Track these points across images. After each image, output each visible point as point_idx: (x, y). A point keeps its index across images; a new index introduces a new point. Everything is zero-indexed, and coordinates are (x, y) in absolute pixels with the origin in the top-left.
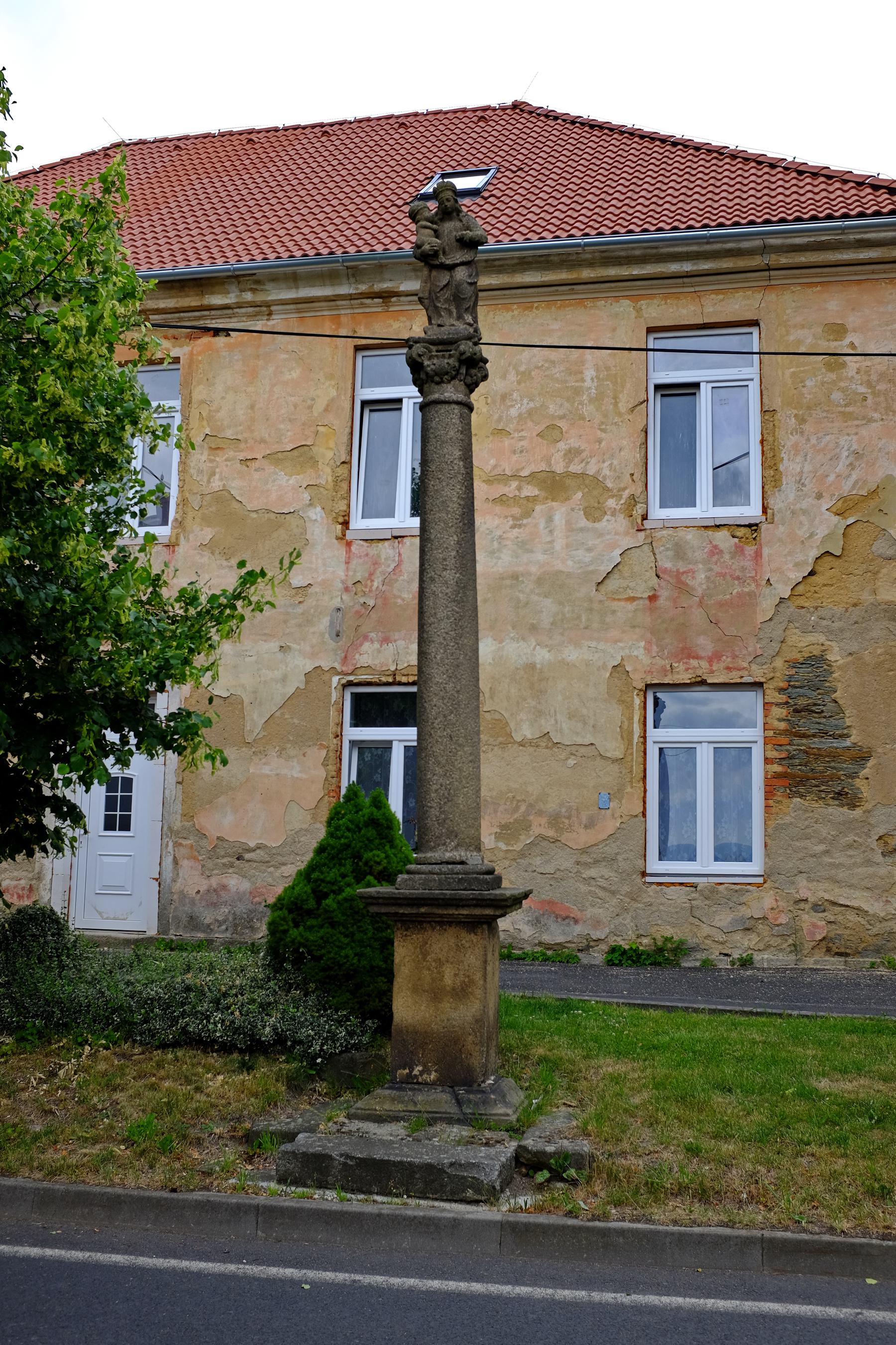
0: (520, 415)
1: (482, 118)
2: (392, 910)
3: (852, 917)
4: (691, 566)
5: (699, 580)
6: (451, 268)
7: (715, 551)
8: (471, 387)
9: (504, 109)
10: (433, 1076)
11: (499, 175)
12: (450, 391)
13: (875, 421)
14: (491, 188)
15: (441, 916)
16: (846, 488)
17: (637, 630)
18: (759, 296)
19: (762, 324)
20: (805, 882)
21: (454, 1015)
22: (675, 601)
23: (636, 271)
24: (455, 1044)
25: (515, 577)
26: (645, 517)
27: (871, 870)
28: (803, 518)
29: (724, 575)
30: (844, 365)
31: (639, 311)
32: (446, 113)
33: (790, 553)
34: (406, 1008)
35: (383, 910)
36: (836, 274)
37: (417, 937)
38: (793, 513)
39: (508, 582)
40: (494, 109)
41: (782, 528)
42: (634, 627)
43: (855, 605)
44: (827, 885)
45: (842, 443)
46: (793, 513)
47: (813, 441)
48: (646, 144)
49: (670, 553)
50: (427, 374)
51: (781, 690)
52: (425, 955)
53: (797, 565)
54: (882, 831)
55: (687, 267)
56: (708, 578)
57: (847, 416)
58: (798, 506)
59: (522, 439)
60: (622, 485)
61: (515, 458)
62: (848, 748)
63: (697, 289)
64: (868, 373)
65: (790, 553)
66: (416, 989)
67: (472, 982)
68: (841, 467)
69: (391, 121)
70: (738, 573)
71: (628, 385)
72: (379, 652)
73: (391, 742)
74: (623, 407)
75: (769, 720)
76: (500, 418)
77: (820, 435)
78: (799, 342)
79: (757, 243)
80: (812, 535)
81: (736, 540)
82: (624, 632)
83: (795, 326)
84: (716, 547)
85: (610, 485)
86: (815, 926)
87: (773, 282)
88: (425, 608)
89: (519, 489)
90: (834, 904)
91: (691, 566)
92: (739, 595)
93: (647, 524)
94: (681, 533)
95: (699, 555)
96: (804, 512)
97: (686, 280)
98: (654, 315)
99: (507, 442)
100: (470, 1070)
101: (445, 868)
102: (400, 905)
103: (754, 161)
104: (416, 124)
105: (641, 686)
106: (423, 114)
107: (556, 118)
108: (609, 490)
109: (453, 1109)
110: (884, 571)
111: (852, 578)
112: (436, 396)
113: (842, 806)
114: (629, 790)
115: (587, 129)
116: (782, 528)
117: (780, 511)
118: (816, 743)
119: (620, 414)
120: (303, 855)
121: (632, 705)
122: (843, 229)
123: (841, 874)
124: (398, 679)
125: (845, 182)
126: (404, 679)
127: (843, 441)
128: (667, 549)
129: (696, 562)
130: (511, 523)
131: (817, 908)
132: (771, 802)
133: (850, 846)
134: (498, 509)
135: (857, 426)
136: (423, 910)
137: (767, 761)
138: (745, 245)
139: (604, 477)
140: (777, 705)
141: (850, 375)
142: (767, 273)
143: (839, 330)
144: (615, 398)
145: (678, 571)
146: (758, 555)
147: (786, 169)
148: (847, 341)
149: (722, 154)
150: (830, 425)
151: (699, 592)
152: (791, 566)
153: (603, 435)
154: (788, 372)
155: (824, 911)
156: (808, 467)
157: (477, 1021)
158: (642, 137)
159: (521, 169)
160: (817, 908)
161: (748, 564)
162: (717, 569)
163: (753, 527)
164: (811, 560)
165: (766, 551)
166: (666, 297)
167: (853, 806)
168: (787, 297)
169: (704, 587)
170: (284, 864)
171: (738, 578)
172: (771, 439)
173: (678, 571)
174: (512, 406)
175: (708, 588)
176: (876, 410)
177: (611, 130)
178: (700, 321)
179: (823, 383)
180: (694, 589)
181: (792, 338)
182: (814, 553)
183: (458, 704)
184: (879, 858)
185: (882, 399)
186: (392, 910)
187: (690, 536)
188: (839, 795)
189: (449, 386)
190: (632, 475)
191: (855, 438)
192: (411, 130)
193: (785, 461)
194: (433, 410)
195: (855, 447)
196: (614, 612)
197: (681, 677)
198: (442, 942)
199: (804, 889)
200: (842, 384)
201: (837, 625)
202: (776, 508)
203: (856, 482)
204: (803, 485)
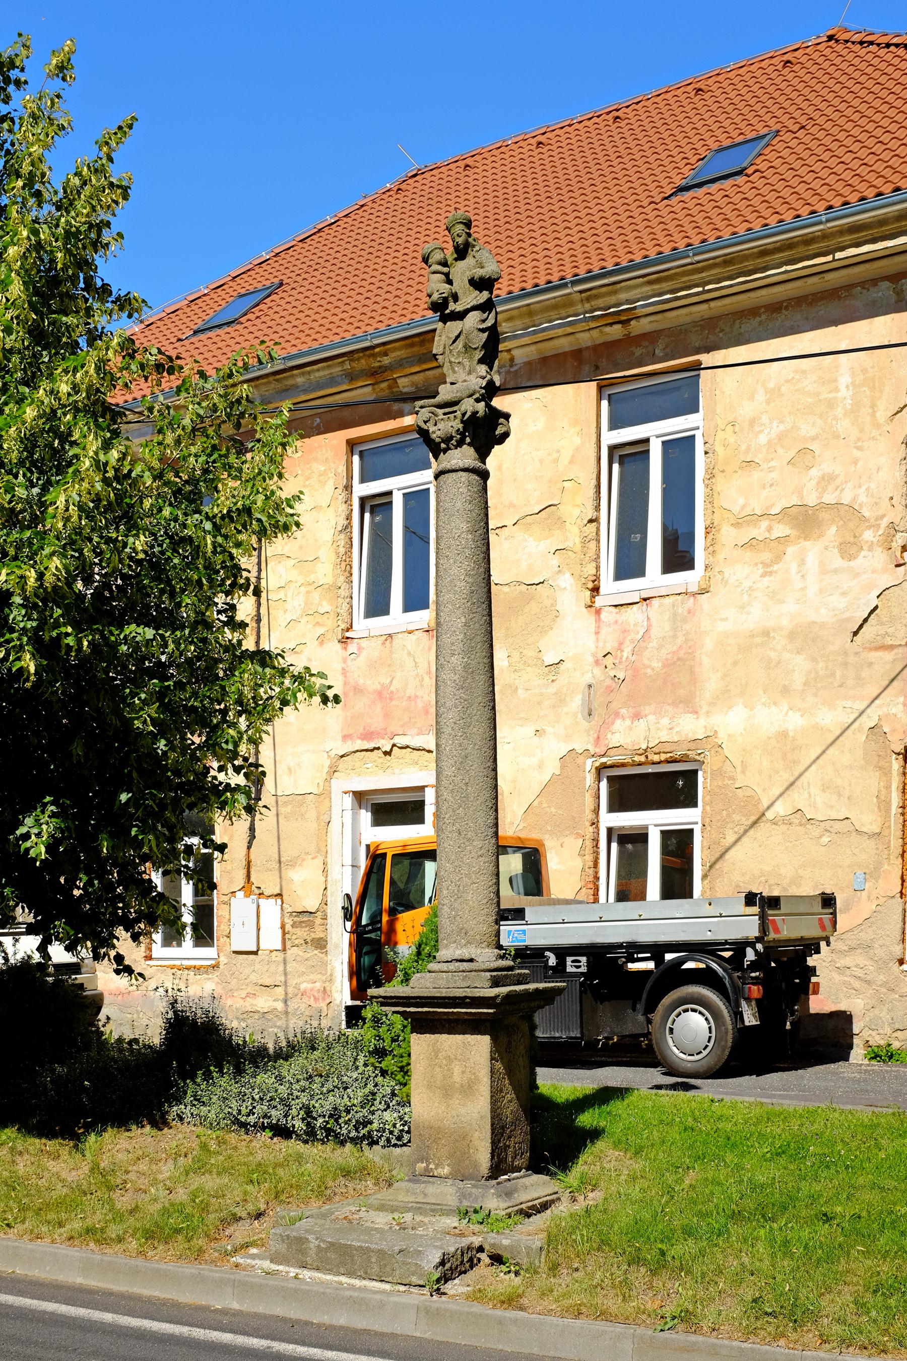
0: (769, 441)
10: (446, 1170)
21: (462, 1111)
25: (766, 633)
39: (759, 640)
59: (771, 470)
60: (880, 513)
73: (646, 827)
76: (749, 447)
89: (769, 529)
99: (756, 475)
114: (886, 867)
119: (877, 426)
126: (656, 758)
130: (761, 571)
134: (748, 555)
144: (873, 406)
174: (761, 432)
196: (870, 664)
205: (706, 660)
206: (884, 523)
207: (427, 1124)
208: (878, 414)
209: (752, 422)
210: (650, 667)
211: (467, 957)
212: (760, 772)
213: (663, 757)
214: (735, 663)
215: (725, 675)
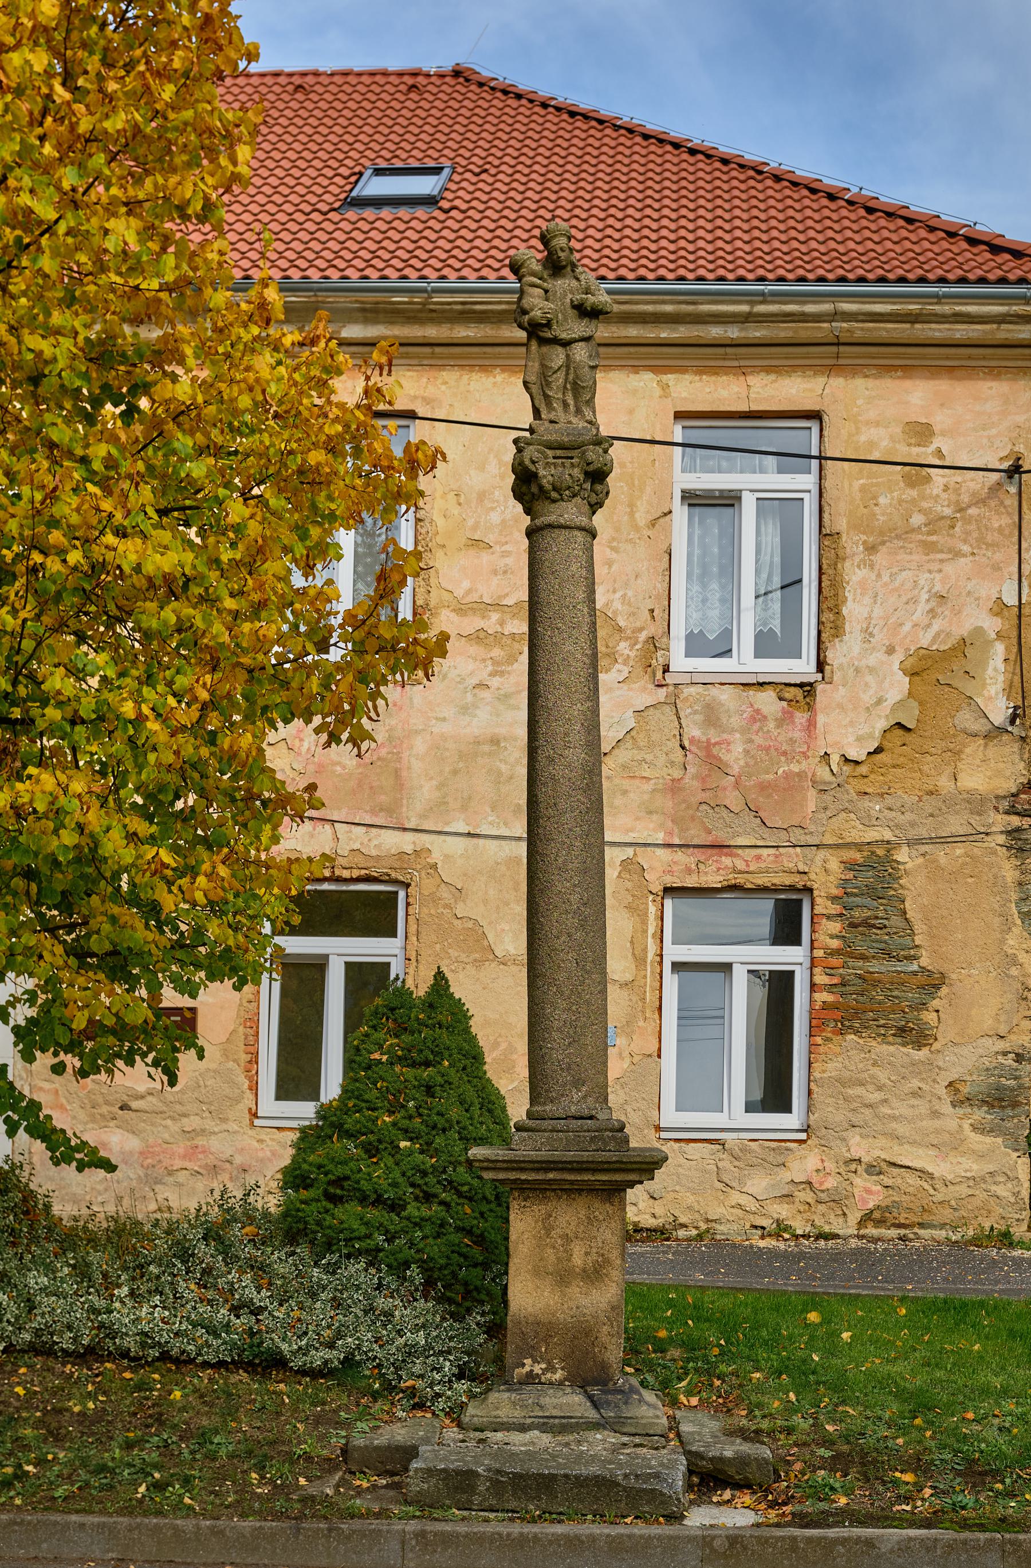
0: (503, 521)
1: (413, 87)
2: (512, 1176)
3: (912, 1180)
4: (725, 736)
5: (735, 756)
6: (566, 344)
7: (757, 717)
8: (595, 507)
9: (442, 76)
10: (558, 1375)
11: (456, 178)
12: (570, 512)
13: (964, 556)
14: (449, 195)
15: (572, 1182)
16: (925, 640)
17: (655, 817)
18: (821, 380)
19: (825, 418)
20: (858, 1138)
21: (584, 1301)
22: (703, 780)
23: (665, 333)
24: (587, 1335)
25: (495, 741)
26: (666, 669)
27: (937, 1123)
28: (869, 678)
29: (767, 749)
30: (928, 479)
31: (665, 387)
32: (359, 74)
33: (852, 723)
34: (527, 1295)
35: (501, 1176)
36: (924, 357)
37: (539, 1209)
38: (857, 670)
39: (486, 748)
40: (428, 75)
41: (842, 691)
42: (651, 813)
43: (931, 793)
44: (882, 1142)
45: (922, 582)
46: (857, 670)
47: (886, 578)
48: (653, 148)
49: (699, 718)
50: (541, 488)
51: (834, 899)
52: (548, 1230)
53: (859, 739)
54: (953, 1076)
55: (733, 333)
56: (747, 752)
57: (929, 548)
58: (863, 663)
59: (506, 554)
60: (638, 624)
61: (495, 581)
62: (915, 973)
63: (742, 363)
64: (957, 491)
65: (852, 723)
66: (537, 1272)
67: (607, 1261)
68: (920, 613)
69: (282, 80)
70: (785, 747)
71: (648, 490)
72: (312, 836)
73: (326, 957)
74: (642, 518)
75: (816, 936)
76: (477, 523)
77: (895, 570)
78: (872, 444)
79: (826, 307)
80: (880, 701)
81: (784, 704)
82: (637, 819)
83: (868, 423)
84: (758, 711)
85: (622, 624)
86: (869, 1191)
87: (841, 362)
88: (541, 797)
89: (502, 623)
90: (894, 1165)
91: (725, 736)
92: (787, 775)
93: (670, 679)
94: (714, 691)
95: (735, 721)
96: (871, 670)
97: (729, 350)
98: (684, 395)
99: (485, 557)
100: (604, 1366)
101: (575, 1124)
102: (522, 1170)
103: (807, 187)
104: (319, 89)
105: (657, 888)
106: (325, 74)
107: (519, 96)
108: (620, 630)
109: (592, 1414)
110: (968, 750)
111: (929, 758)
112: (552, 518)
113: (904, 1045)
114: (641, 1023)
115: (565, 116)
116: (842, 691)
117: (841, 667)
118: (874, 966)
119: (637, 528)
120: (211, 1103)
121: (646, 914)
122: (938, 298)
123: (901, 1129)
124: (337, 873)
125: (932, 229)
126: (346, 874)
127: (924, 578)
128: (695, 712)
129: (733, 731)
130: (490, 668)
131: (872, 1169)
132: (819, 1040)
133: (914, 1094)
134: (473, 649)
135: (942, 561)
136: (551, 1176)
137: (813, 987)
138: (810, 308)
139: (615, 612)
140: (829, 917)
141: (935, 492)
142: (834, 349)
143: (922, 432)
144: (631, 505)
145: (708, 741)
146: (811, 724)
147: (850, 202)
148: (933, 447)
149: (760, 172)
150: (908, 557)
151: (735, 770)
152: (851, 739)
153: (614, 556)
154: (858, 484)
155: (880, 1173)
156: (878, 612)
157: (613, 1308)
158: (646, 137)
159: (486, 171)
160: (872, 1169)
161: (797, 735)
162: (759, 740)
163: (807, 688)
164: (878, 734)
165: (821, 719)
166: (701, 371)
167: (919, 1046)
168: (859, 383)
169: (742, 763)
170: (185, 1115)
171: (785, 753)
172: (831, 572)
173: (708, 741)
174: (493, 509)
175: (747, 764)
176: (965, 541)
177: (601, 122)
178: (744, 408)
179: (901, 501)
180: (727, 766)
181: (863, 438)
182: (882, 724)
183: (585, 920)
184: (947, 1109)
185: (973, 527)
186: (512, 1176)
187: (725, 696)
188: (902, 1031)
189: (570, 505)
190: (652, 611)
191: (938, 577)
192: (314, 97)
193: (849, 603)
194: (548, 536)
195: (938, 587)
196: (625, 792)
197: (710, 878)
198: (568, 1216)
199: (859, 1147)
200: (925, 505)
201: (909, 816)
202: (836, 664)
203: (938, 634)
204: (871, 635)
205: (417, 765)
206: (643, 636)
207: (531, 1319)
208: (637, 515)
209: (482, 496)
210: (339, 763)
211: (586, 1112)
212: (485, 902)
213: (356, 873)
214: (455, 772)
215: (441, 786)
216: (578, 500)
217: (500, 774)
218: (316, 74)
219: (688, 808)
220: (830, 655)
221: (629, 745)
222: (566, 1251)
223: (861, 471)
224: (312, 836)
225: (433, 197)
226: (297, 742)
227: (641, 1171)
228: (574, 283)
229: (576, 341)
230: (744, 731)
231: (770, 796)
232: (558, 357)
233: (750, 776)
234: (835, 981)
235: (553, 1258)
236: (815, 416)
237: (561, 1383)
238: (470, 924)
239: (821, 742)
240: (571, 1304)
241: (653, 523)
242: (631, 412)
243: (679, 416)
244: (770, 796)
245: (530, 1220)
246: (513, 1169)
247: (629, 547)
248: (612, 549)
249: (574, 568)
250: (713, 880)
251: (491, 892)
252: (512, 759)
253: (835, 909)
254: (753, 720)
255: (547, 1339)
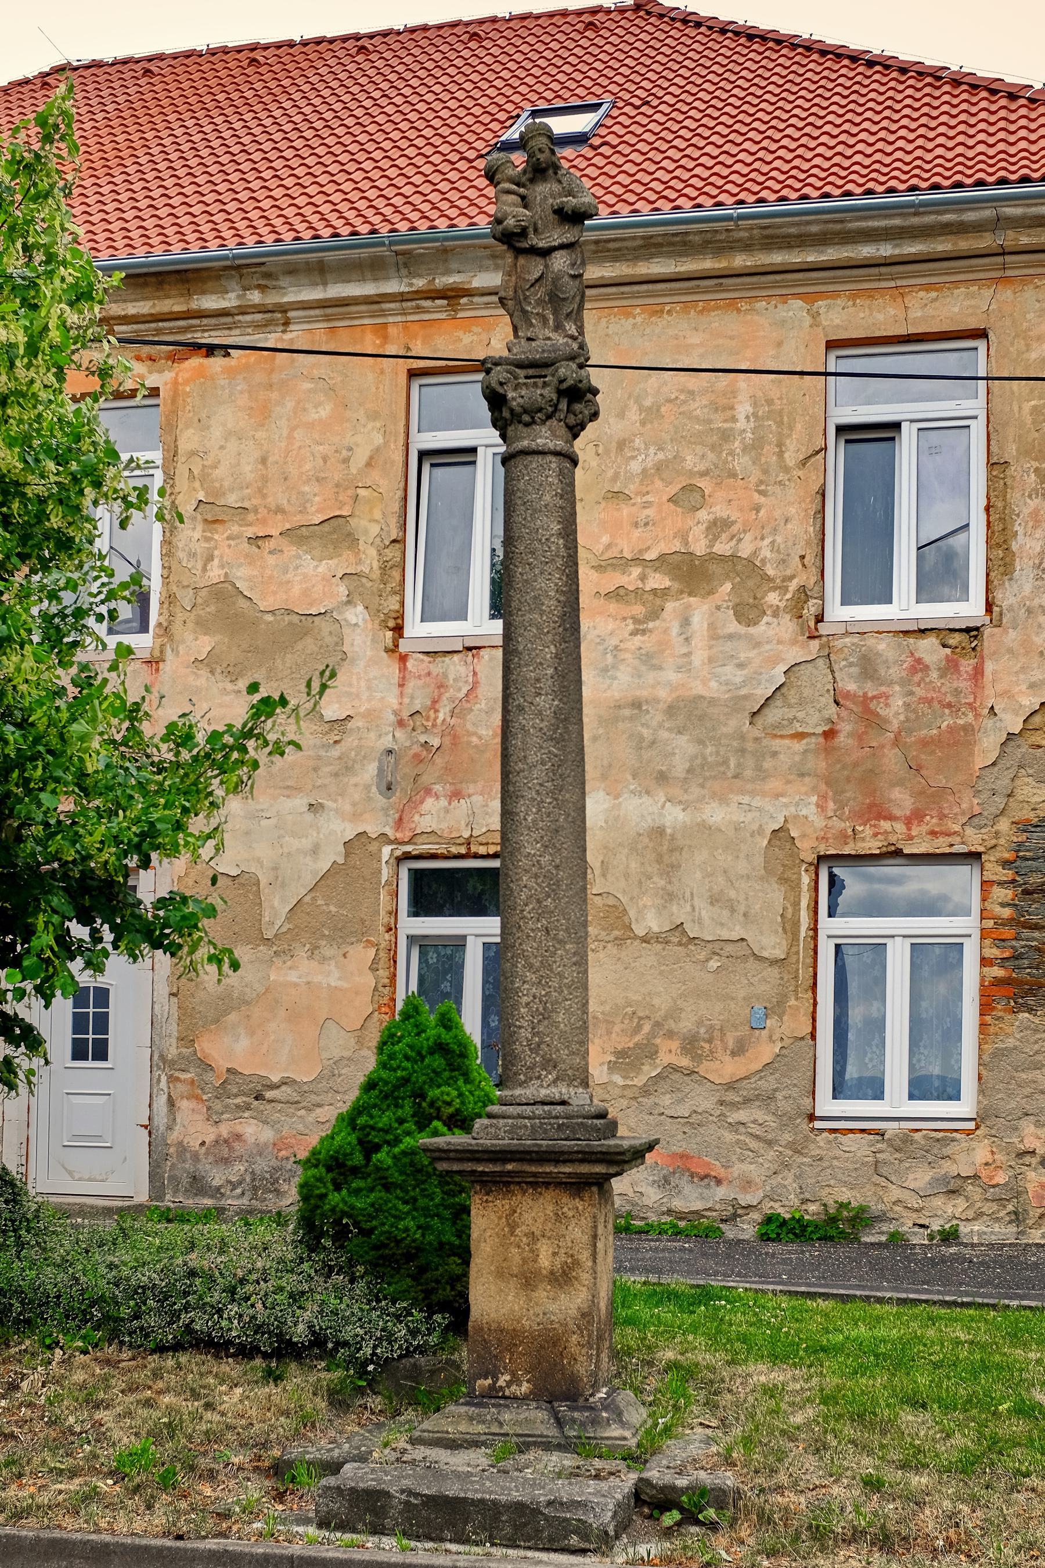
0: (644, 471)
2: (468, 1166)
4: (883, 689)
5: (894, 709)
6: (545, 253)
7: (919, 666)
8: (575, 431)
9: (622, 11)
10: (525, 1387)
11: (615, 113)
12: (545, 437)
14: (603, 131)
15: (535, 1175)
17: (807, 779)
18: (987, 293)
19: (991, 335)
20: (1032, 1128)
21: (553, 1307)
25: (637, 705)
26: (820, 619)
29: (929, 701)
31: (815, 315)
32: (538, 17)
34: (489, 1299)
35: (456, 1167)
37: (503, 1204)
38: (1029, 611)
39: (627, 712)
40: (608, 12)
46: (1029, 611)
50: (512, 410)
51: (1006, 864)
52: (513, 1227)
55: (886, 250)
56: (907, 705)
59: (647, 505)
60: (788, 572)
61: (637, 533)
63: (899, 283)
65: (1023, 669)
67: (577, 1263)
70: (949, 698)
72: (447, 811)
73: (464, 937)
74: (791, 458)
79: (988, 213)
81: (948, 651)
82: (788, 782)
84: (919, 661)
88: (511, 750)
89: (643, 578)
91: (883, 689)
92: (951, 729)
94: (870, 641)
97: (883, 270)
98: (837, 321)
99: (626, 511)
101: (539, 1110)
102: (479, 1160)
105: (811, 857)
106: (503, 19)
107: (698, 25)
108: (770, 579)
109: (551, 1431)
114: (793, 1002)
115: (742, 40)
117: (1011, 609)
119: (786, 469)
124: (474, 849)
126: (482, 850)
128: (851, 664)
129: (892, 683)
130: (631, 627)
132: (988, 1018)
134: (613, 607)
136: (509, 1167)
137: (984, 962)
138: (970, 216)
140: (1000, 884)
144: (780, 445)
146: (978, 672)
152: (1024, 687)
153: (763, 500)
154: (1027, 407)
157: (584, 1315)
158: (823, 53)
159: (647, 103)
161: (964, 684)
162: (920, 692)
163: (972, 632)
165: (989, 667)
169: (902, 718)
170: (320, 1106)
171: (949, 705)
174: (633, 458)
175: (907, 720)
178: (902, 331)
183: (558, 884)
187: (883, 646)
194: (520, 463)
196: (775, 754)
197: (867, 845)
198: (535, 1211)
206: (793, 585)
209: (621, 445)
210: (475, 734)
212: (627, 876)
216: (554, 422)
217: (641, 739)
218: (494, 20)
219: (844, 768)
220: (999, 595)
221: (779, 703)
222: (532, 1251)
223: (1032, 391)
224: (447, 811)
225: (584, 134)
226: (432, 713)
227: (610, 1162)
228: (556, 187)
229: (554, 249)
230: (903, 682)
231: (933, 752)
232: (535, 268)
233: (910, 731)
234: (1006, 955)
235: (517, 1259)
236: (982, 334)
237: (525, 1398)
238: (611, 901)
239: (989, 691)
240: (539, 1310)
241: (804, 462)
242: (780, 344)
243: (831, 345)
244: (933, 752)
245: (493, 1216)
246: (469, 1160)
247: (778, 489)
248: (760, 492)
249: (547, 498)
250: (872, 846)
251: (633, 865)
252: (654, 723)
253: (1008, 874)
254: (913, 670)
255: (511, 1348)
